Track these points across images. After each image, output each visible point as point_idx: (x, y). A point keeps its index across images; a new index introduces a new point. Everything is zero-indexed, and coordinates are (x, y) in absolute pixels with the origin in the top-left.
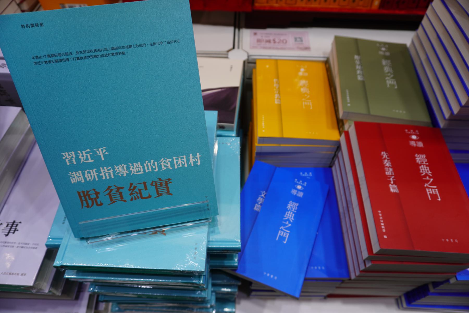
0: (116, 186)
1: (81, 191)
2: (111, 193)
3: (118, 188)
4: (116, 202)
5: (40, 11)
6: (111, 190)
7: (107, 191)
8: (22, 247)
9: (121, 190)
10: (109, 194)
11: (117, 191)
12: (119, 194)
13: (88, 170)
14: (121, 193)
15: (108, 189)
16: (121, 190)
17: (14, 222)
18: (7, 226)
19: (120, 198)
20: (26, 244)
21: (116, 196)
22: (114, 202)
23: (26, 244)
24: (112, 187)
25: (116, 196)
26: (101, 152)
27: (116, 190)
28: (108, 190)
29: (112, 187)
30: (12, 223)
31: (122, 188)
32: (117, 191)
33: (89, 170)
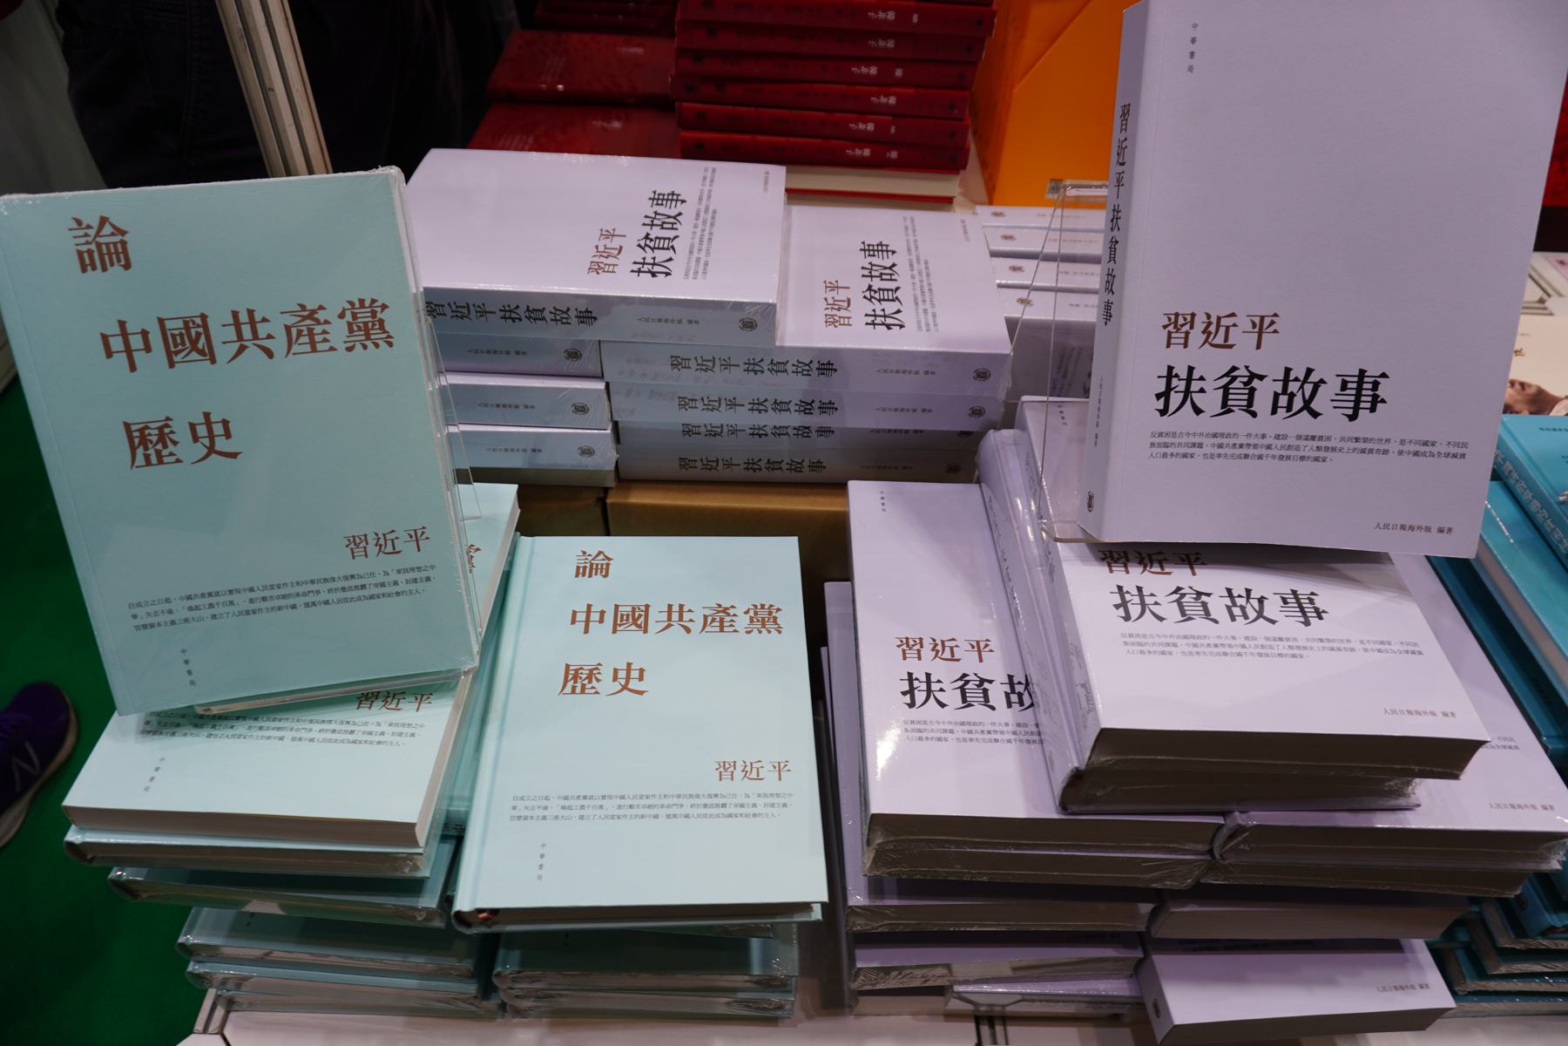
0: (1250, 368)
1: (198, 314)
2: (1230, 386)
3: (982, 681)
4: (1232, 411)
5: (1088, 655)
6: (967, 682)
7: (1225, 378)
8: (1416, 454)
9: (986, 685)
10: (962, 689)
11: (1245, 384)
12: (981, 691)
13: (1222, 862)
14: (985, 691)
15: (960, 679)
16: (986, 685)
17: (1362, 373)
18: (1344, 386)
19: (982, 699)
20: (1425, 443)
21: (974, 695)
22: (970, 705)
23: (1425, 443)
24: (1238, 369)
25: (974, 695)
26: (1504, 437)
27: (978, 683)
28: (1228, 376)
29: (1238, 369)
30: (1356, 379)
31: (991, 682)
32: (1245, 384)
33: (1495, 518)
